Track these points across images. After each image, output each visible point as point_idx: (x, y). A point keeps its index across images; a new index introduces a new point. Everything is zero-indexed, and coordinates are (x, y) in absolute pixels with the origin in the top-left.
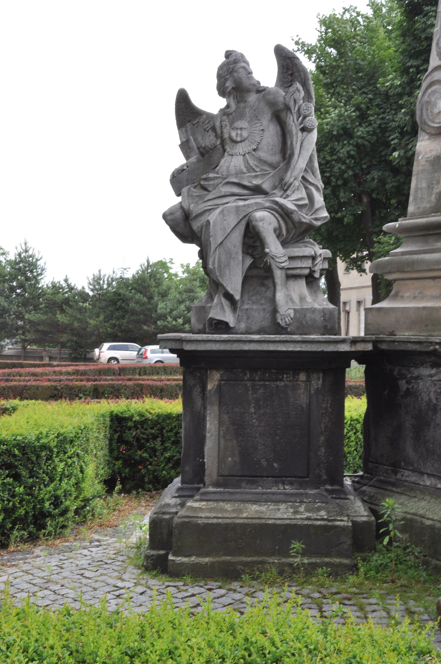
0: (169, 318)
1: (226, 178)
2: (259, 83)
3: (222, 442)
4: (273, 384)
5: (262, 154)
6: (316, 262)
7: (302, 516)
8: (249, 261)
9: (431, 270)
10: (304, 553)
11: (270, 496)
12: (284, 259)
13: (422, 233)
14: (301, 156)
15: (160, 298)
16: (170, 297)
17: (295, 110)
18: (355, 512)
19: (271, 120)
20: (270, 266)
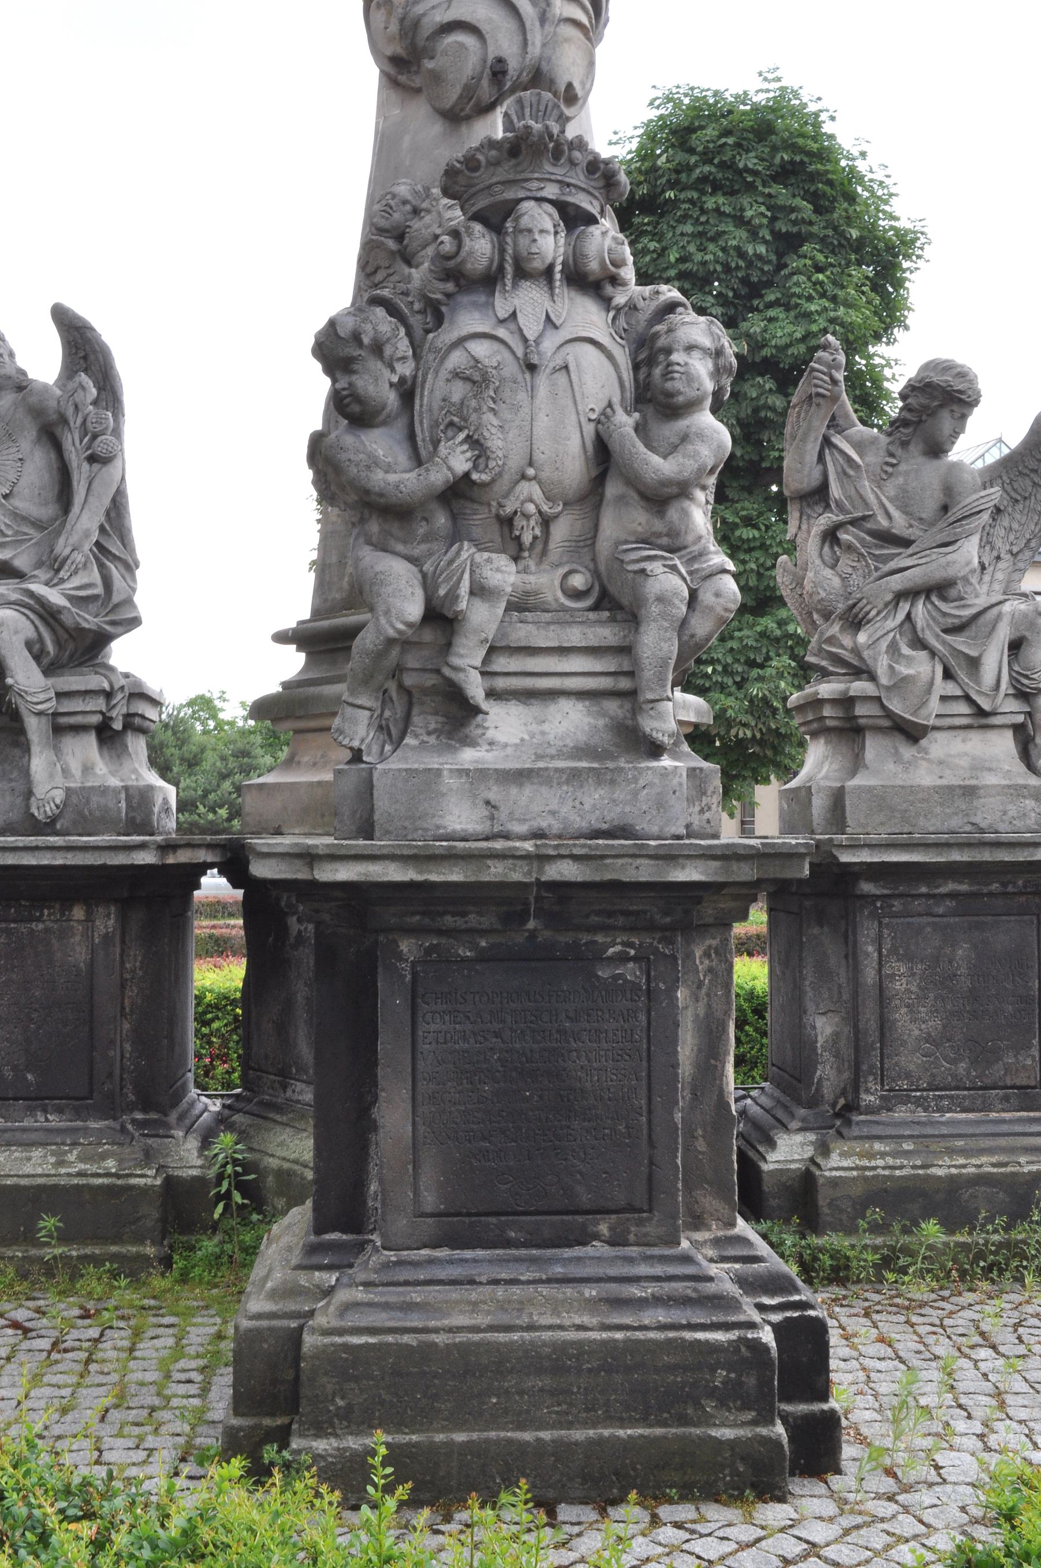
0: (201, 807)
2: (24, 373)
4: (23, 928)
5: (22, 504)
6: (114, 702)
7: (70, 1170)
10: (64, 1237)
11: (18, 1135)
13: (329, 646)
14: (86, 507)
15: (184, 767)
16: (206, 765)
17: (76, 422)
18: (181, 1159)
19: (39, 439)
20: (17, 708)
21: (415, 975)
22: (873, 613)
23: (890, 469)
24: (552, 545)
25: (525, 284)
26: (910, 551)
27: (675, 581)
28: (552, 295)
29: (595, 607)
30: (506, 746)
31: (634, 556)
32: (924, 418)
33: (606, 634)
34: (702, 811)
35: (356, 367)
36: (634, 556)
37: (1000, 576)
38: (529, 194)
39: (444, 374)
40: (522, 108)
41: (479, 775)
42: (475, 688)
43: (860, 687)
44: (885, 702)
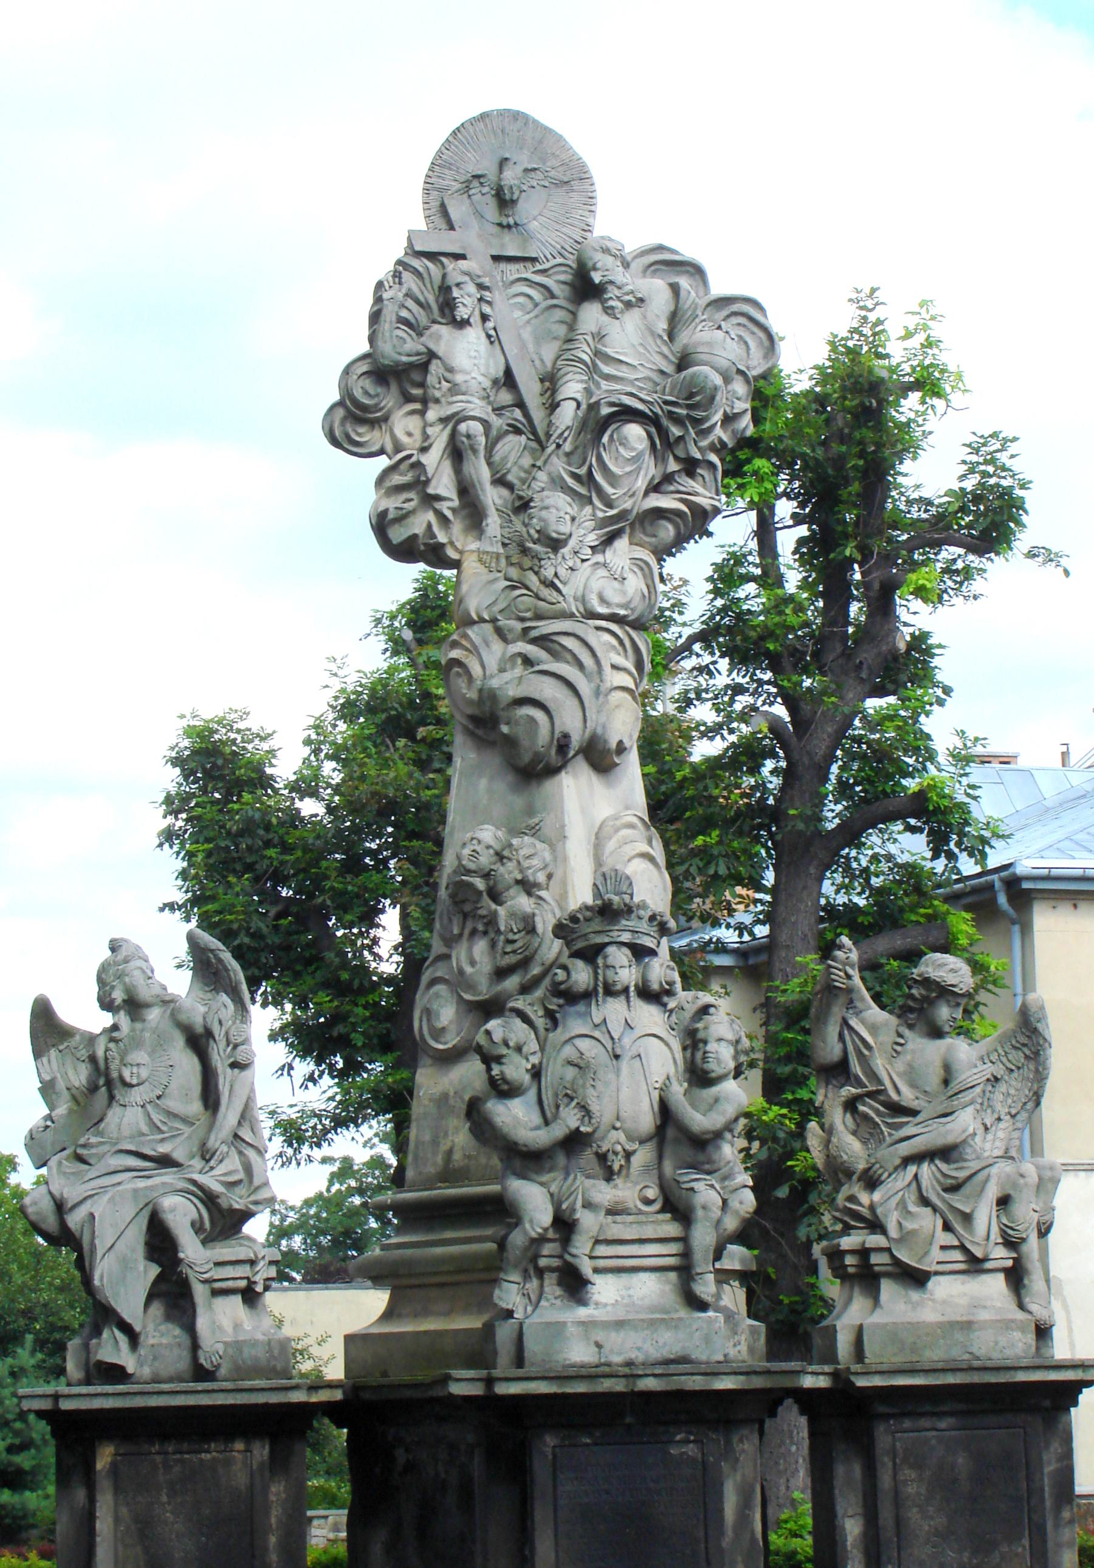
1: (116, 1144)
3: (120, 1548)
4: (193, 1457)
5: (173, 1104)
8: (155, 1270)
9: (436, 1274)
12: (207, 1267)
20: (187, 1277)
21: (555, 1456)
22: (886, 1175)
23: (898, 1048)
24: (632, 1170)
25: (610, 999)
26: (919, 1118)
27: (713, 1193)
28: (629, 1006)
29: (663, 1210)
30: (606, 1305)
31: (686, 1178)
32: (925, 1005)
33: (672, 1229)
34: (735, 1345)
35: (504, 1060)
36: (686, 1178)
37: (1001, 1134)
38: (612, 940)
39: (560, 1061)
40: (605, 879)
41: (587, 1325)
42: (586, 1267)
43: (875, 1240)
44: (895, 1253)
